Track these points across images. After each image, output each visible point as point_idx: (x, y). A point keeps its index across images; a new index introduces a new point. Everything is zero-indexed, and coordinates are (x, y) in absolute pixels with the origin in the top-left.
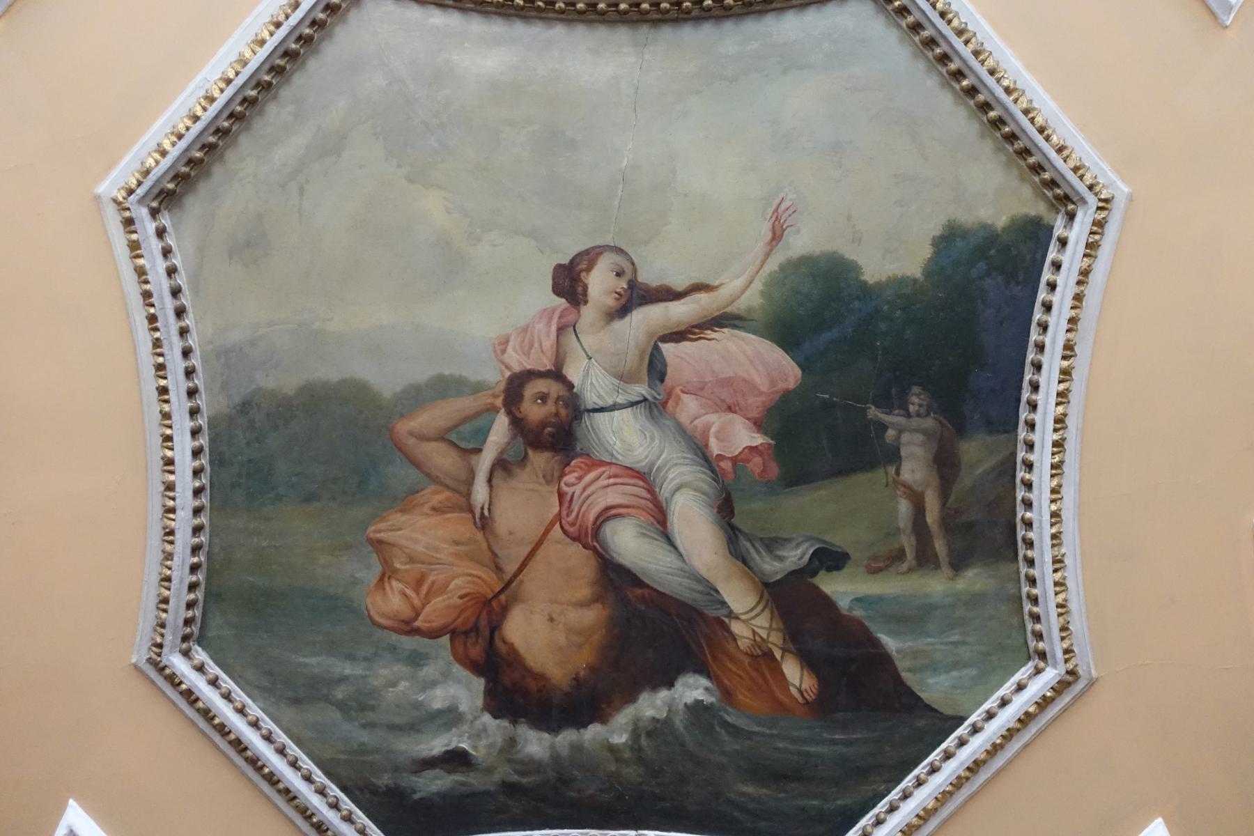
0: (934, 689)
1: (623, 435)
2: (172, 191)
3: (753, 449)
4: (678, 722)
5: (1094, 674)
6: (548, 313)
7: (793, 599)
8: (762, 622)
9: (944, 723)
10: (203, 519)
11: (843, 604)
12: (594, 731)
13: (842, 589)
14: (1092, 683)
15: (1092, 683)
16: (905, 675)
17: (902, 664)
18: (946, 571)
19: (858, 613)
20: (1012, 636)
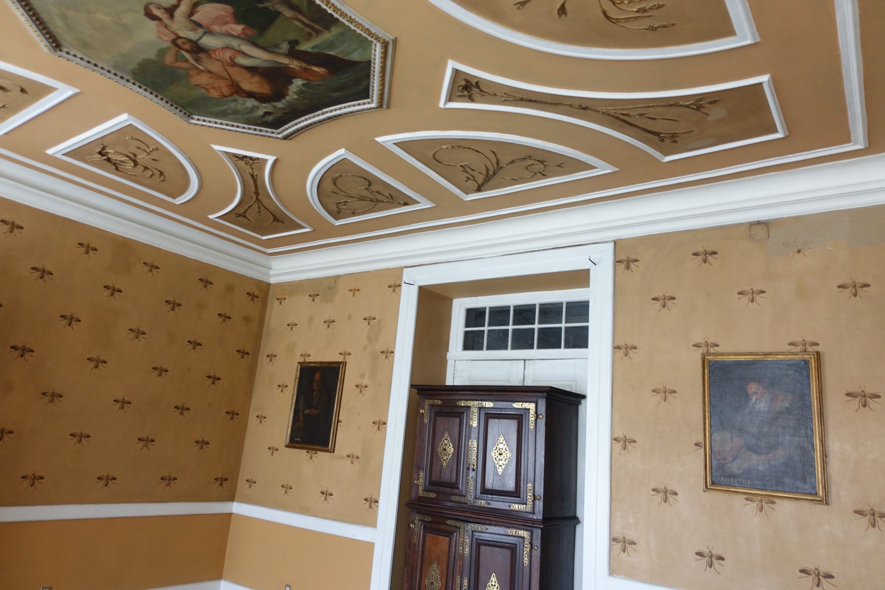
0: (355, 57)
1: (208, 41)
2: (56, 44)
3: (243, 29)
4: (303, 88)
5: (392, 38)
6: (157, 25)
7: (293, 53)
8: (295, 62)
9: (368, 64)
10: (160, 97)
11: (310, 50)
12: (287, 98)
13: (306, 47)
14: (395, 41)
15: (395, 41)
16: (345, 58)
17: (341, 56)
18: (326, 32)
19: (316, 50)
20: (364, 44)
